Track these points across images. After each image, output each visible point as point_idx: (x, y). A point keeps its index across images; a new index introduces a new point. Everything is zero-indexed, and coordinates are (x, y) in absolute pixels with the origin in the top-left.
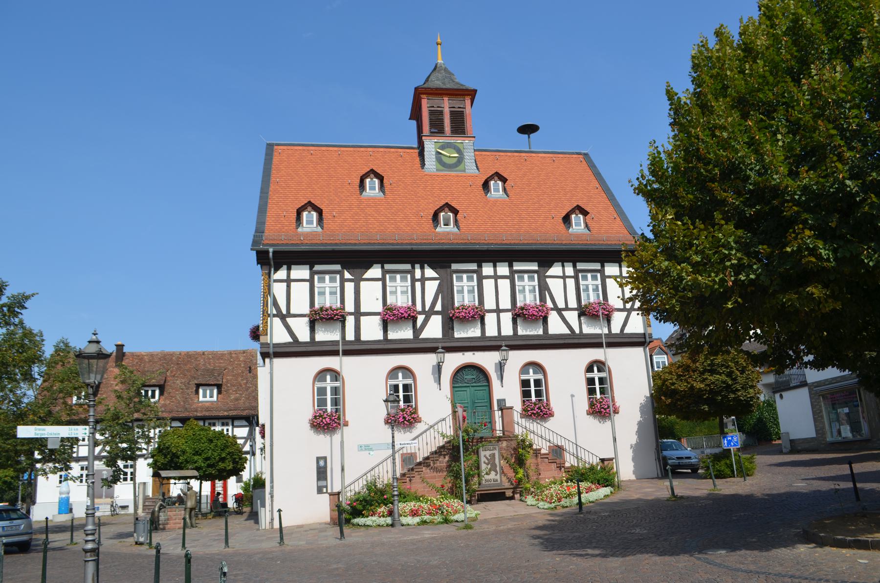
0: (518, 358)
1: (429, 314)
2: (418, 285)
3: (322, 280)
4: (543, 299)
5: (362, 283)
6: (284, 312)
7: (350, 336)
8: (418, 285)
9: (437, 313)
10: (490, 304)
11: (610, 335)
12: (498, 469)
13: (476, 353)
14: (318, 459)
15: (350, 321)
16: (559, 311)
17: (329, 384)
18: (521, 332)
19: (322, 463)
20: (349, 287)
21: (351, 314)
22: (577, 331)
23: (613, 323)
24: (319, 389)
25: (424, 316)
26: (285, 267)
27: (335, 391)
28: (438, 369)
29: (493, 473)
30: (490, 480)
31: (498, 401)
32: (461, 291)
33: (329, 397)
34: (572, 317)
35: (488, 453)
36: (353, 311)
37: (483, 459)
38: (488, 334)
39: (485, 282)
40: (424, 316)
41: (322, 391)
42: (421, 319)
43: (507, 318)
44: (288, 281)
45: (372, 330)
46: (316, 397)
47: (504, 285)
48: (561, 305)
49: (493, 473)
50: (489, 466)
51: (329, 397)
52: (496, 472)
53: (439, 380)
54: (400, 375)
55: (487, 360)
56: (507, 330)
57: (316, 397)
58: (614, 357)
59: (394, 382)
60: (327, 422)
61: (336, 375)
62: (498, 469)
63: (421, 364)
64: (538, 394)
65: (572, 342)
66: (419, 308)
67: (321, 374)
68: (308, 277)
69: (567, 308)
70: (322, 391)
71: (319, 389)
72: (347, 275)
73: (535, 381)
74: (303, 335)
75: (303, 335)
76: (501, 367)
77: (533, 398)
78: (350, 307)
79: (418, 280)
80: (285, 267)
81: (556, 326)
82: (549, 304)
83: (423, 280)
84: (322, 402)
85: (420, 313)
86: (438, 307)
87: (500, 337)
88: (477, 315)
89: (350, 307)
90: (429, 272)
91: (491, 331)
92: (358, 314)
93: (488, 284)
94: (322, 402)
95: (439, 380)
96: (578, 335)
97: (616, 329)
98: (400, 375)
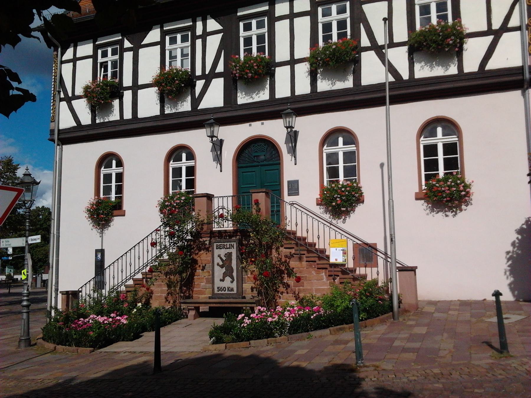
0: (312, 127)
1: (208, 78)
2: (199, 42)
3: (173, 41)
4: (356, 34)
5: (141, 51)
6: (70, 95)
7: (128, 115)
8: (199, 42)
9: (219, 75)
10: (282, 53)
11: (461, 75)
12: (235, 274)
13: (266, 122)
14: (97, 251)
15: (128, 95)
16: (379, 50)
17: (341, 148)
18: (167, 111)
19: (99, 256)
20: (128, 57)
21: (128, 88)
22: (405, 76)
23: (466, 55)
24: (426, 147)
25: (203, 81)
26: (72, 45)
27: (450, 148)
28: (218, 146)
29: (228, 279)
30: (224, 289)
31: (289, 182)
32: (248, 41)
33: (441, 157)
34: (399, 57)
35: (223, 252)
36: (130, 84)
37: (217, 260)
38: (466, 70)
39: (278, 25)
40: (203, 81)
41: (333, 158)
42: (200, 84)
43: (302, 70)
44: (74, 60)
45: (149, 104)
46: (325, 166)
47: (303, 25)
48: (381, 40)
49: (228, 279)
50: (224, 270)
51: (441, 157)
52: (232, 278)
53: (218, 158)
54: (439, 130)
55: (274, 130)
56: (303, 87)
57: (422, 159)
58: (361, 121)
59: (430, 141)
60: (104, 212)
61: (350, 137)
62: (235, 274)
63: (197, 139)
64: (451, 164)
65: (406, 91)
66: (199, 72)
67: (428, 128)
68: (91, 53)
69: (392, 45)
70: (431, 150)
71: (426, 147)
72: (127, 44)
73: (445, 146)
74: (86, 119)
75: (86, 119)
76: (293, 137)
77: (441, 172)
78: (127, 81)
79: (199, 37)
80: (72, 45)
81: (372, 71)
82: (365, 41)
83: (205, 34)
84: (333, 173)
85: (200, 78)
86: (220, 68)
87: (294, 98)
88: (263, 71)
89: (127, 81)
90: (213, 25)
91: (283, 91)
92: (136, 87)
93: (282, 28)
94: (333, 173)
95: (218, 158)
96: (406, 81)
97: (471, 65)
98: (439, 130)
